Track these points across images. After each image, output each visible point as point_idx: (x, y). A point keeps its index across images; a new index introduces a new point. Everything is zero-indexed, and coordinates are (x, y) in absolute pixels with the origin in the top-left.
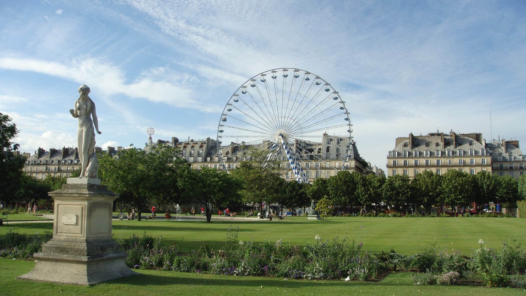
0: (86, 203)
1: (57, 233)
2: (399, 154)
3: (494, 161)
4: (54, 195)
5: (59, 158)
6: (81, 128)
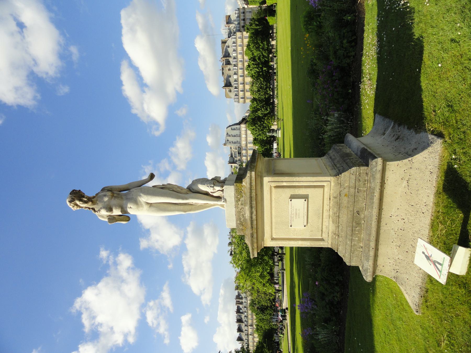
0: (266, 180)
1: (322, 240)
2: (236, 95)
3: (239, 31)
4: (255, 245)
5: (243, 325)
6: (142, 206)
